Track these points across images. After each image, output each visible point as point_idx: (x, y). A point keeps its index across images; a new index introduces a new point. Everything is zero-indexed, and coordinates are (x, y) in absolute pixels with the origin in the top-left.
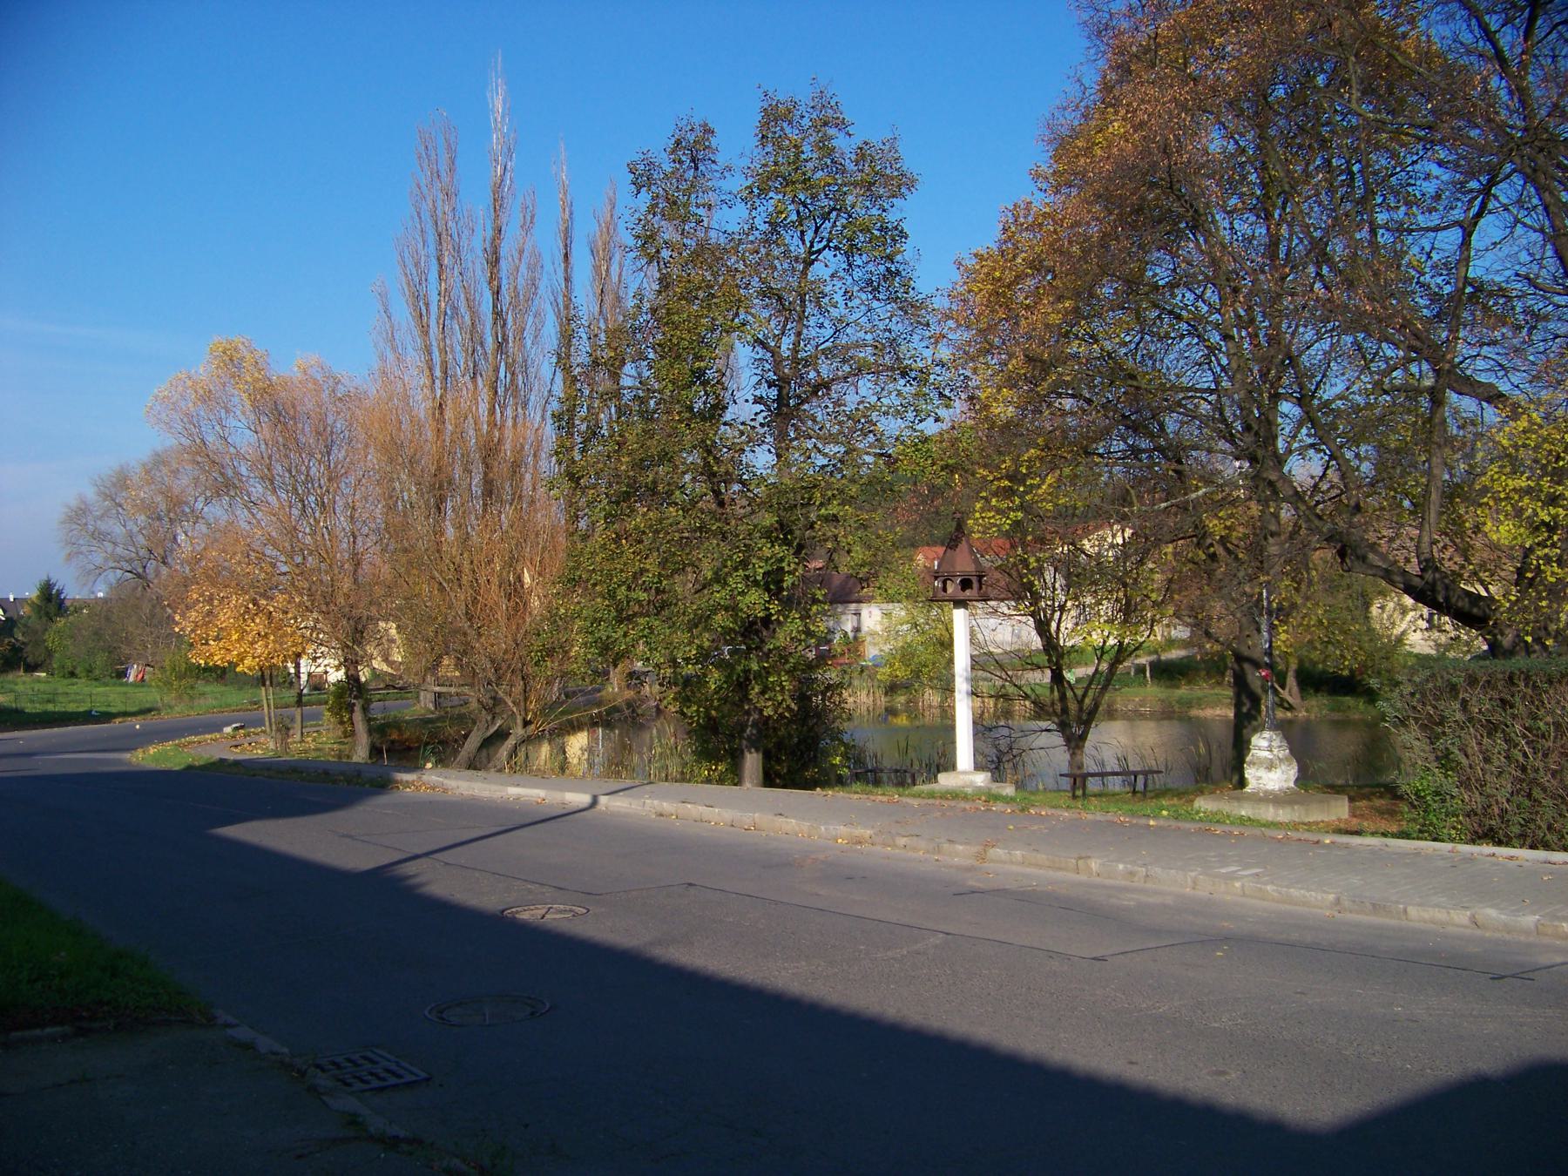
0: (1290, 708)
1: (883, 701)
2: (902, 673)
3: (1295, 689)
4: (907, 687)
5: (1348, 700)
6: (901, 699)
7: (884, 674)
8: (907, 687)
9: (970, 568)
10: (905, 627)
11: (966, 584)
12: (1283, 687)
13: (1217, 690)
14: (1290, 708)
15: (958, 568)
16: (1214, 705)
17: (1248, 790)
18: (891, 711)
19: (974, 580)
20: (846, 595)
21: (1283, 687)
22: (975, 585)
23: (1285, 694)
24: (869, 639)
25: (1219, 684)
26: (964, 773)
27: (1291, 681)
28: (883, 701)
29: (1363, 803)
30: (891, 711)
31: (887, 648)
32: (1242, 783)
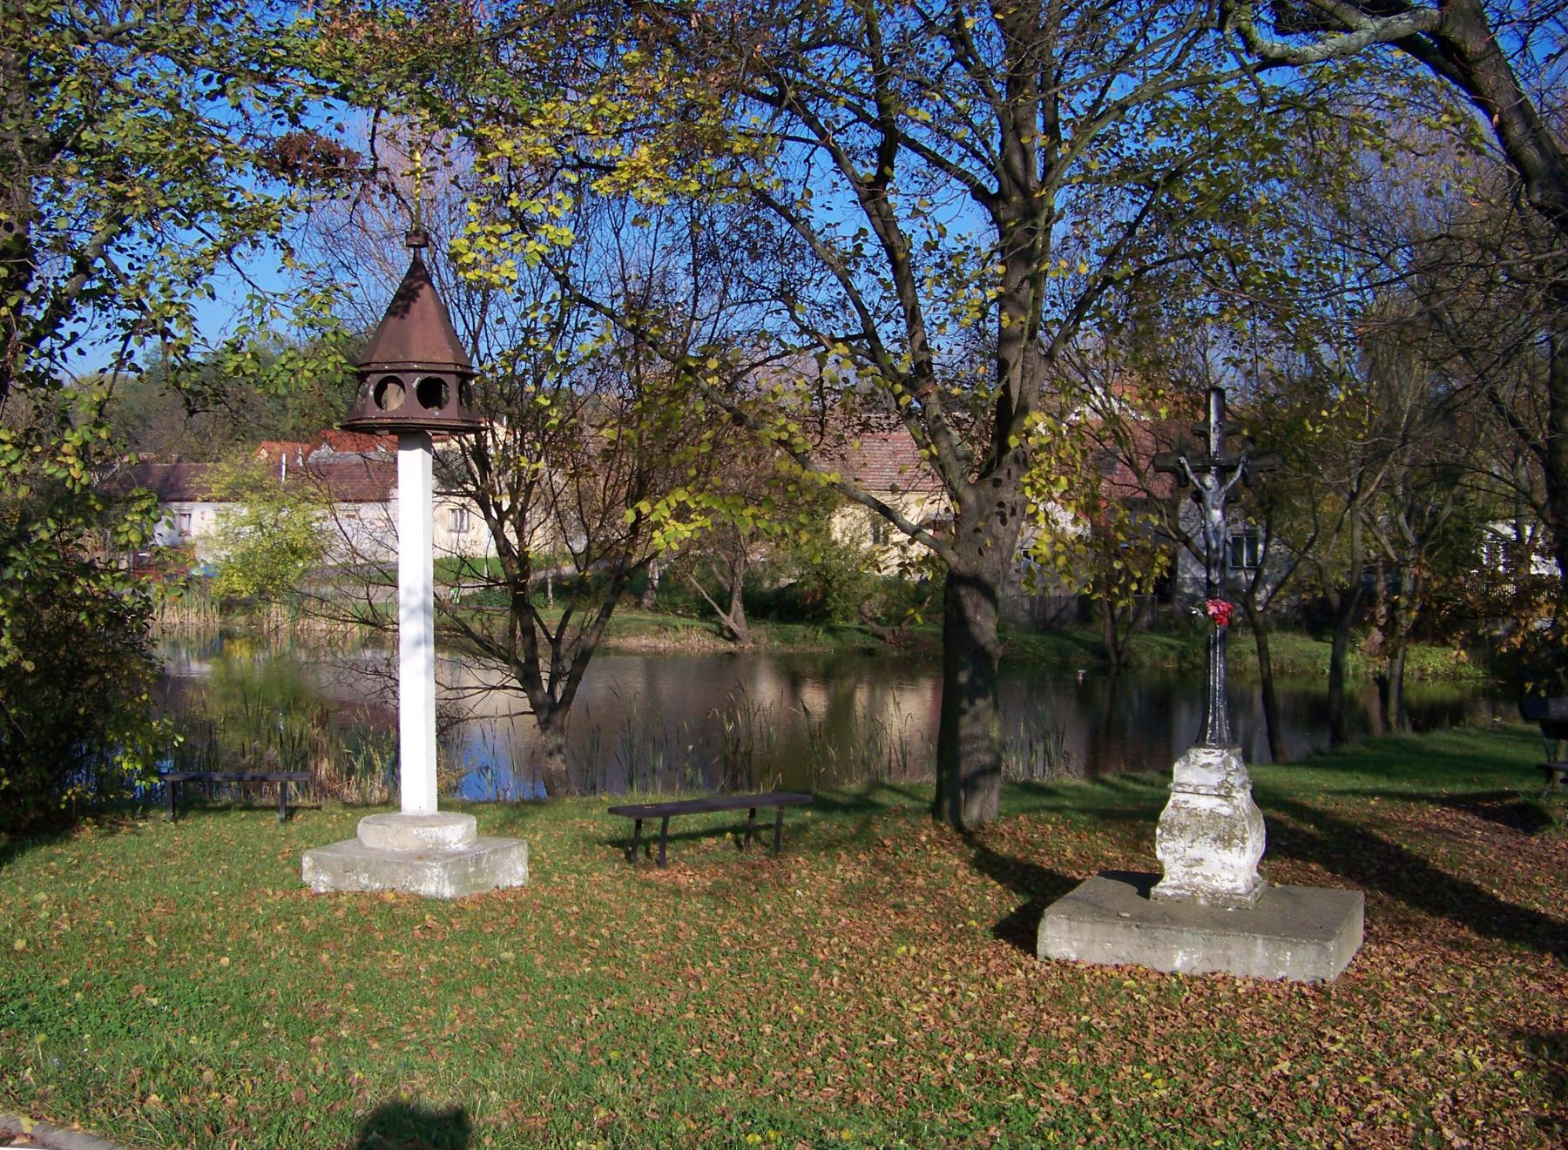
0: (734, 637)
1: (217, 621)
2: (245, 589)
3: (741, 615)
4: (248, 606)
5: (799, 629)
6: (239, 621)
7: (219, 587)
8: (248, 606)
9: (443, 356)
10: (247, 529)
11: (430, 393)
12: (727, 610)
13: (636, 614)
14: (734, 637)
15: (417, 355)
16: (639, 632)
17: (1163, 888)
18: (227, 635)
19: (452, 382)
20: (171, 491)
21: (727, 610)
22: (453, 394)
23: (728, 621)
24: (200, 543)
25: (638, 605)
26: (419, 820)
27: (737, 605)
28: (217, 621)
29: (446, 656)
30: (227, 635)
31: (223, 554)
32: (1146, 880)
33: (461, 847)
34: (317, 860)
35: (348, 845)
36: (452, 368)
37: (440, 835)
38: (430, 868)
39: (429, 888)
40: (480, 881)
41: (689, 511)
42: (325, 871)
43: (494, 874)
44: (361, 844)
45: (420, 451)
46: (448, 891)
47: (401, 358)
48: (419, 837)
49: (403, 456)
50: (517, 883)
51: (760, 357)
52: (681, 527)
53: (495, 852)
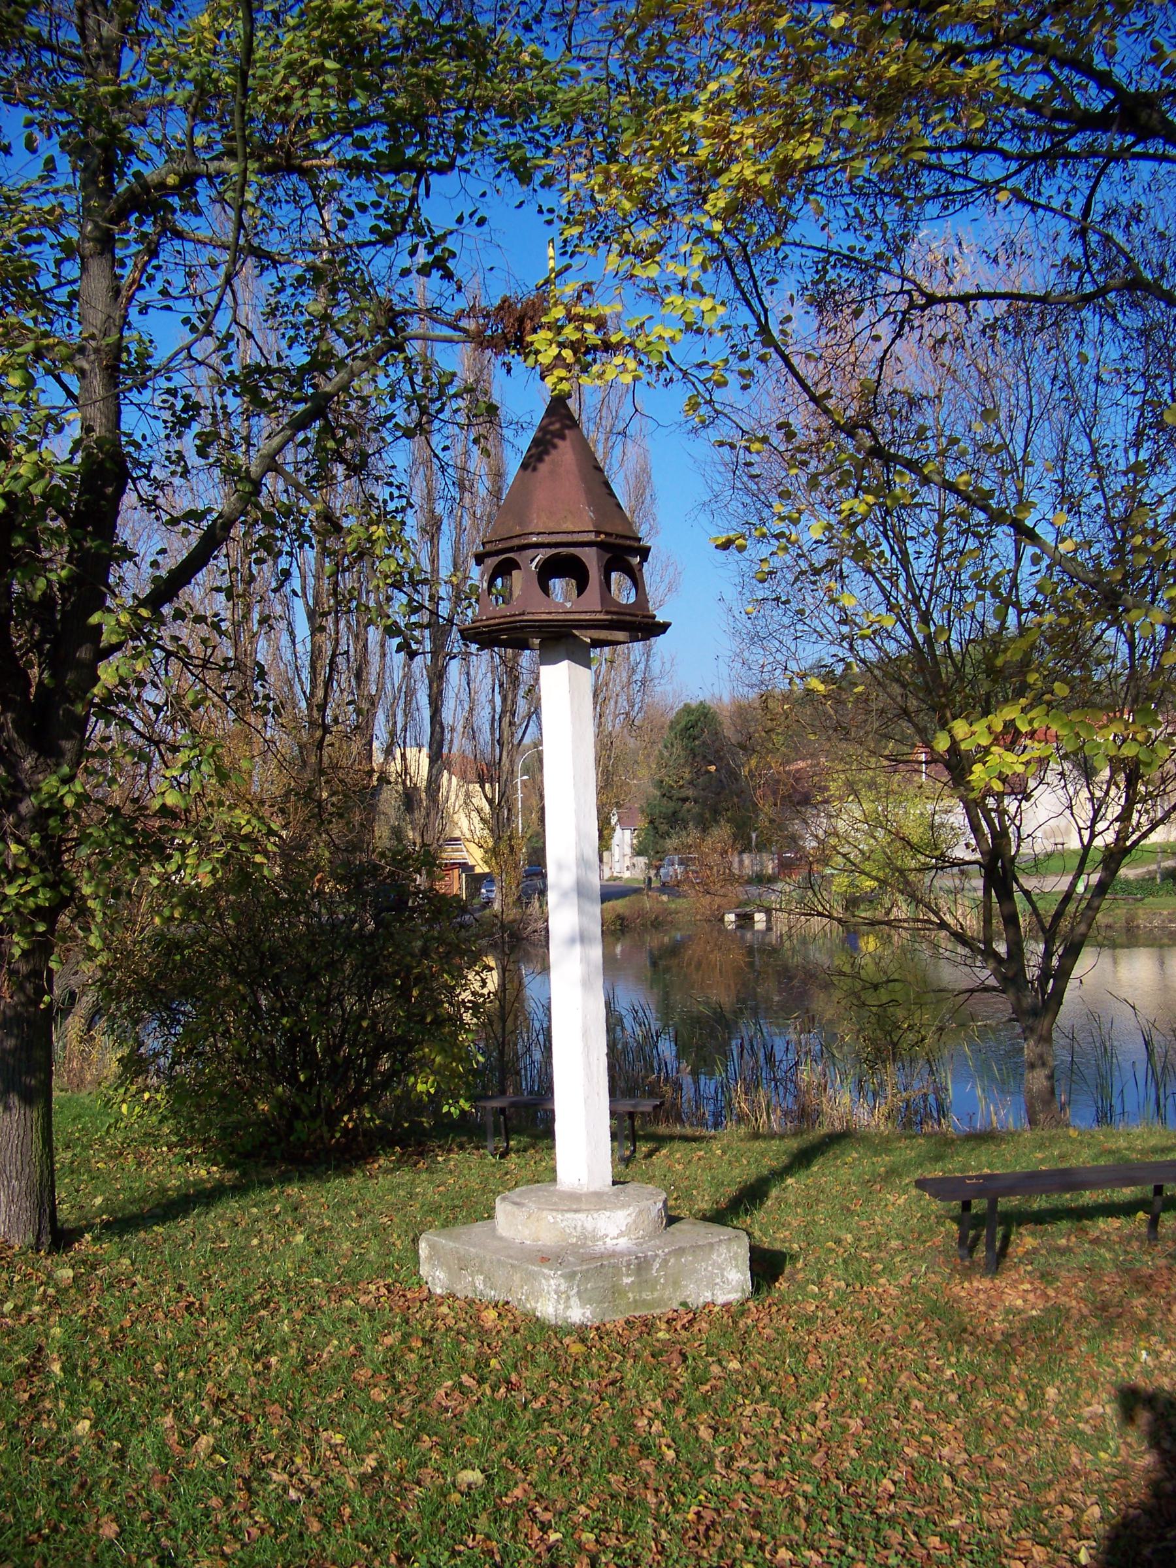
26: (575, 1201)
33: (623, 1243)
34: (432, 1247)
35: (479, 1228)
36: (592, 537)
37: (589, 1225)
38: (547, 1278)
39: (547, 1309)
40: (647, 1296)
41: (1018, 733)
42: (441, 1265)
43: (676, 1284)
44: (494, 1229)
45: (565, 664)
46: (578, 1314)
47: (518, 530)
48: (572, 1226)
49: (546, 671)
50: (734, 1297)
51: (756, 272)
52: (1010, 757)
53: (681, 1251)
